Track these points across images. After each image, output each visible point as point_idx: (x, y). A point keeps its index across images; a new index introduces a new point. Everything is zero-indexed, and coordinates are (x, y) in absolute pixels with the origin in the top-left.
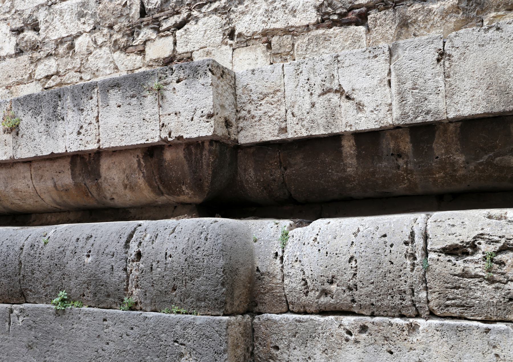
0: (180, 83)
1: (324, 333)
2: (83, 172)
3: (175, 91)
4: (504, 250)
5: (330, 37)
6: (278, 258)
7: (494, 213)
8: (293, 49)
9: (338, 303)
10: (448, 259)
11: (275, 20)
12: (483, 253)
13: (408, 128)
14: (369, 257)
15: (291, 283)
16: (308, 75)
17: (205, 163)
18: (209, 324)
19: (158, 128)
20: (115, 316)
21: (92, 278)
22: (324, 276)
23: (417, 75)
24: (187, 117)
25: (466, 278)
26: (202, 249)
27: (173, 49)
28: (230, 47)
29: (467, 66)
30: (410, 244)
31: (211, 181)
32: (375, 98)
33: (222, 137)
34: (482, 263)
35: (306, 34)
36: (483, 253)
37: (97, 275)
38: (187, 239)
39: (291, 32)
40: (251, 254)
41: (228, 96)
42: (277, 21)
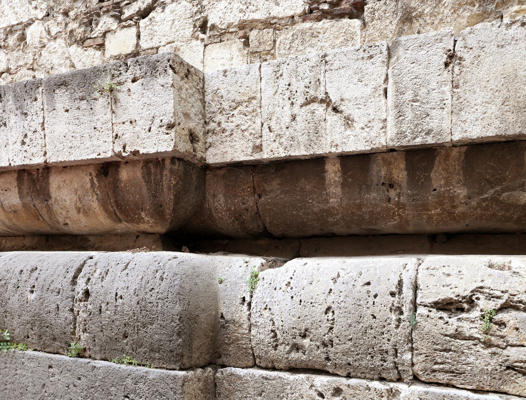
0: (136, 83)
1: (293, 394)
2: (31, 190)
3: (130, 93)
4: (506, 308)
5: (319, 33)
6: (246, 304)
7: (496, 261)
8: (274, 47)
9: (310, 360)
10: (440, 316)
11: (254, 8)
12: (482, 311)
13: (404, 151)
14: (349, 308)
15: (258, 333)
16: (289, 79)
17: (165, 186)
18: (162, 379)
19: (111, 139)
20: (61, 363)
21: (36, 318)
22: (296, 328)
23: (419, 84)
24: (144, 127)
25: (458, 339)
26: (156, 291)
27: (136, 43)
28: (202, 42)
29: (481, 73)
30: (397, 296)
31: (174, 208)
32: (367, 112)
33: (186, 153)
34: (479, 323)
35: (290, 28)
36: (482, 311)
37: (41, 314)
38: (140, 277)
39: (273, 24)
40: (215, 298)
41: (194, 102)
42: (257, 10)
